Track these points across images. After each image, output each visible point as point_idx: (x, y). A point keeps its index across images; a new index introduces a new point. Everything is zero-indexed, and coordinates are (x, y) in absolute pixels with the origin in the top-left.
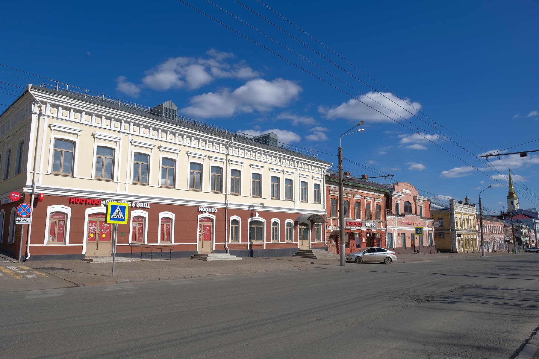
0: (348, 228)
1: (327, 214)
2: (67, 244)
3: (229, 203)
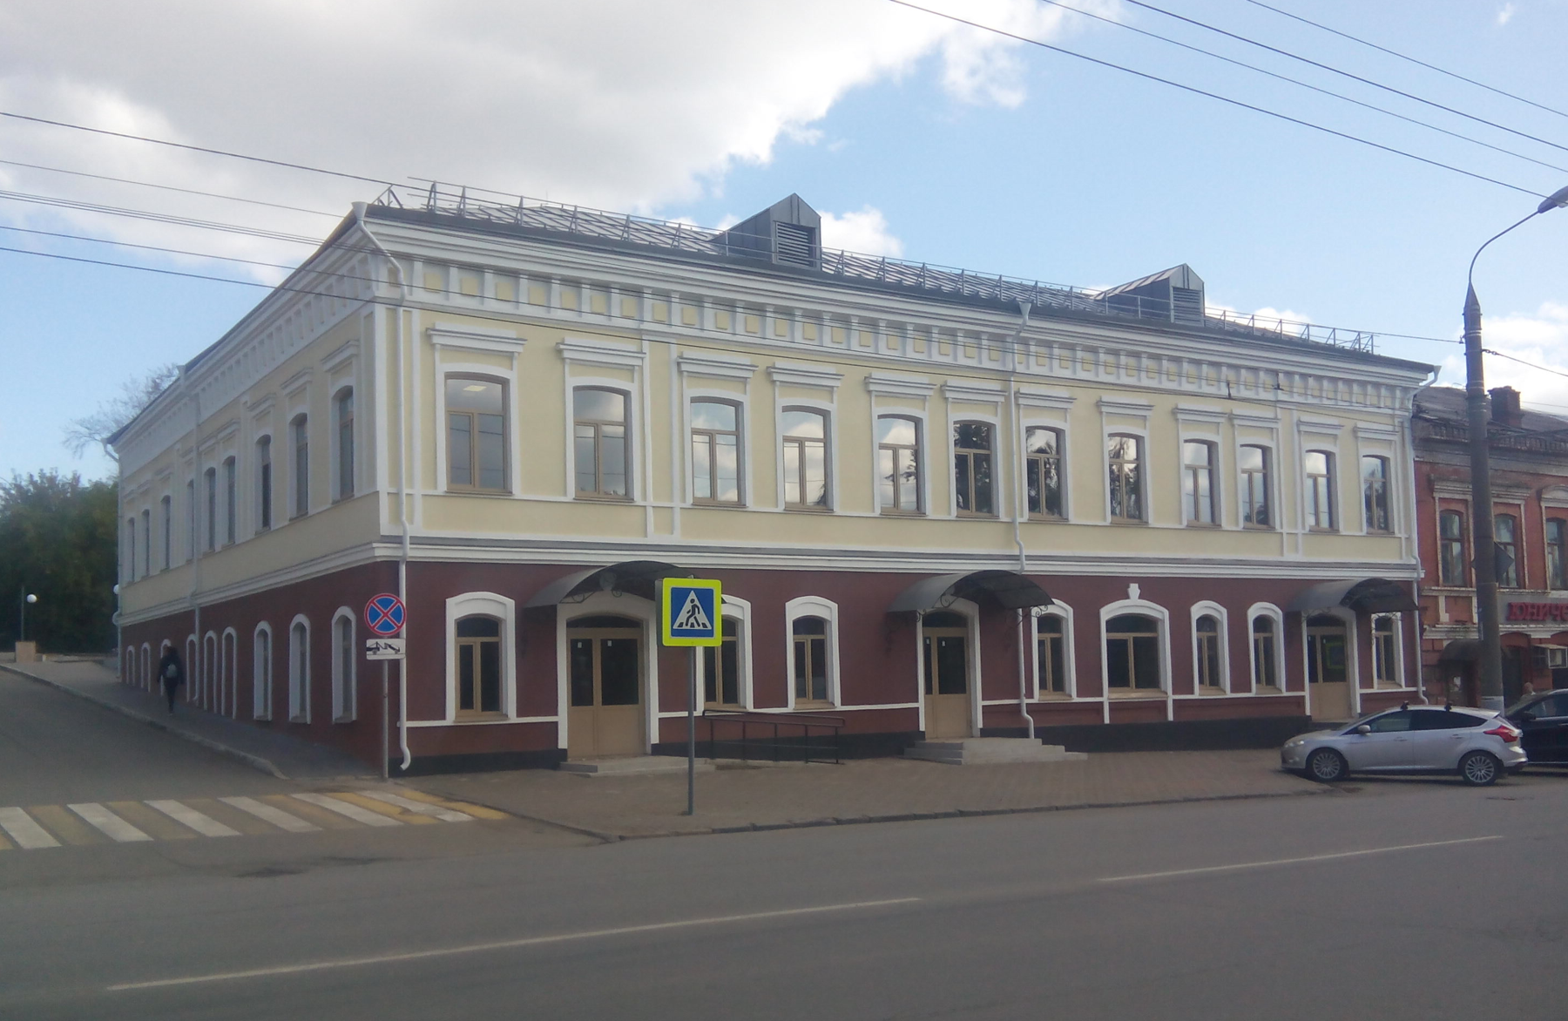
0: (1516, 627)
1: (1422, 576)
2: (513, 718)
3: (1025, 552)
